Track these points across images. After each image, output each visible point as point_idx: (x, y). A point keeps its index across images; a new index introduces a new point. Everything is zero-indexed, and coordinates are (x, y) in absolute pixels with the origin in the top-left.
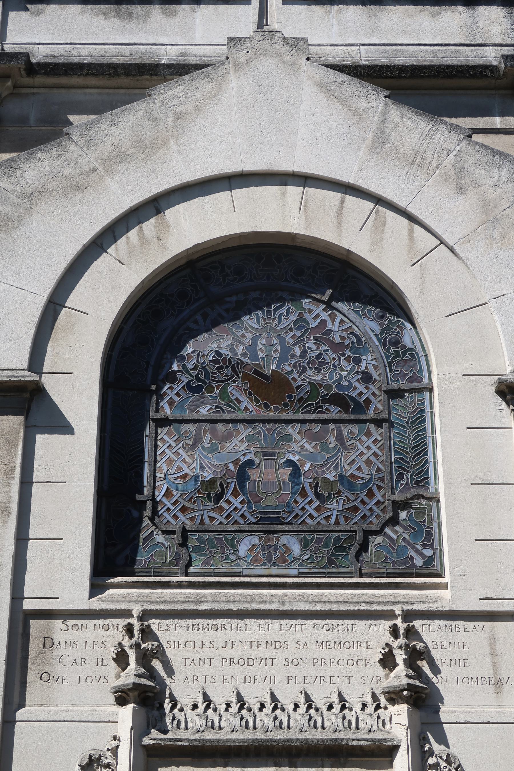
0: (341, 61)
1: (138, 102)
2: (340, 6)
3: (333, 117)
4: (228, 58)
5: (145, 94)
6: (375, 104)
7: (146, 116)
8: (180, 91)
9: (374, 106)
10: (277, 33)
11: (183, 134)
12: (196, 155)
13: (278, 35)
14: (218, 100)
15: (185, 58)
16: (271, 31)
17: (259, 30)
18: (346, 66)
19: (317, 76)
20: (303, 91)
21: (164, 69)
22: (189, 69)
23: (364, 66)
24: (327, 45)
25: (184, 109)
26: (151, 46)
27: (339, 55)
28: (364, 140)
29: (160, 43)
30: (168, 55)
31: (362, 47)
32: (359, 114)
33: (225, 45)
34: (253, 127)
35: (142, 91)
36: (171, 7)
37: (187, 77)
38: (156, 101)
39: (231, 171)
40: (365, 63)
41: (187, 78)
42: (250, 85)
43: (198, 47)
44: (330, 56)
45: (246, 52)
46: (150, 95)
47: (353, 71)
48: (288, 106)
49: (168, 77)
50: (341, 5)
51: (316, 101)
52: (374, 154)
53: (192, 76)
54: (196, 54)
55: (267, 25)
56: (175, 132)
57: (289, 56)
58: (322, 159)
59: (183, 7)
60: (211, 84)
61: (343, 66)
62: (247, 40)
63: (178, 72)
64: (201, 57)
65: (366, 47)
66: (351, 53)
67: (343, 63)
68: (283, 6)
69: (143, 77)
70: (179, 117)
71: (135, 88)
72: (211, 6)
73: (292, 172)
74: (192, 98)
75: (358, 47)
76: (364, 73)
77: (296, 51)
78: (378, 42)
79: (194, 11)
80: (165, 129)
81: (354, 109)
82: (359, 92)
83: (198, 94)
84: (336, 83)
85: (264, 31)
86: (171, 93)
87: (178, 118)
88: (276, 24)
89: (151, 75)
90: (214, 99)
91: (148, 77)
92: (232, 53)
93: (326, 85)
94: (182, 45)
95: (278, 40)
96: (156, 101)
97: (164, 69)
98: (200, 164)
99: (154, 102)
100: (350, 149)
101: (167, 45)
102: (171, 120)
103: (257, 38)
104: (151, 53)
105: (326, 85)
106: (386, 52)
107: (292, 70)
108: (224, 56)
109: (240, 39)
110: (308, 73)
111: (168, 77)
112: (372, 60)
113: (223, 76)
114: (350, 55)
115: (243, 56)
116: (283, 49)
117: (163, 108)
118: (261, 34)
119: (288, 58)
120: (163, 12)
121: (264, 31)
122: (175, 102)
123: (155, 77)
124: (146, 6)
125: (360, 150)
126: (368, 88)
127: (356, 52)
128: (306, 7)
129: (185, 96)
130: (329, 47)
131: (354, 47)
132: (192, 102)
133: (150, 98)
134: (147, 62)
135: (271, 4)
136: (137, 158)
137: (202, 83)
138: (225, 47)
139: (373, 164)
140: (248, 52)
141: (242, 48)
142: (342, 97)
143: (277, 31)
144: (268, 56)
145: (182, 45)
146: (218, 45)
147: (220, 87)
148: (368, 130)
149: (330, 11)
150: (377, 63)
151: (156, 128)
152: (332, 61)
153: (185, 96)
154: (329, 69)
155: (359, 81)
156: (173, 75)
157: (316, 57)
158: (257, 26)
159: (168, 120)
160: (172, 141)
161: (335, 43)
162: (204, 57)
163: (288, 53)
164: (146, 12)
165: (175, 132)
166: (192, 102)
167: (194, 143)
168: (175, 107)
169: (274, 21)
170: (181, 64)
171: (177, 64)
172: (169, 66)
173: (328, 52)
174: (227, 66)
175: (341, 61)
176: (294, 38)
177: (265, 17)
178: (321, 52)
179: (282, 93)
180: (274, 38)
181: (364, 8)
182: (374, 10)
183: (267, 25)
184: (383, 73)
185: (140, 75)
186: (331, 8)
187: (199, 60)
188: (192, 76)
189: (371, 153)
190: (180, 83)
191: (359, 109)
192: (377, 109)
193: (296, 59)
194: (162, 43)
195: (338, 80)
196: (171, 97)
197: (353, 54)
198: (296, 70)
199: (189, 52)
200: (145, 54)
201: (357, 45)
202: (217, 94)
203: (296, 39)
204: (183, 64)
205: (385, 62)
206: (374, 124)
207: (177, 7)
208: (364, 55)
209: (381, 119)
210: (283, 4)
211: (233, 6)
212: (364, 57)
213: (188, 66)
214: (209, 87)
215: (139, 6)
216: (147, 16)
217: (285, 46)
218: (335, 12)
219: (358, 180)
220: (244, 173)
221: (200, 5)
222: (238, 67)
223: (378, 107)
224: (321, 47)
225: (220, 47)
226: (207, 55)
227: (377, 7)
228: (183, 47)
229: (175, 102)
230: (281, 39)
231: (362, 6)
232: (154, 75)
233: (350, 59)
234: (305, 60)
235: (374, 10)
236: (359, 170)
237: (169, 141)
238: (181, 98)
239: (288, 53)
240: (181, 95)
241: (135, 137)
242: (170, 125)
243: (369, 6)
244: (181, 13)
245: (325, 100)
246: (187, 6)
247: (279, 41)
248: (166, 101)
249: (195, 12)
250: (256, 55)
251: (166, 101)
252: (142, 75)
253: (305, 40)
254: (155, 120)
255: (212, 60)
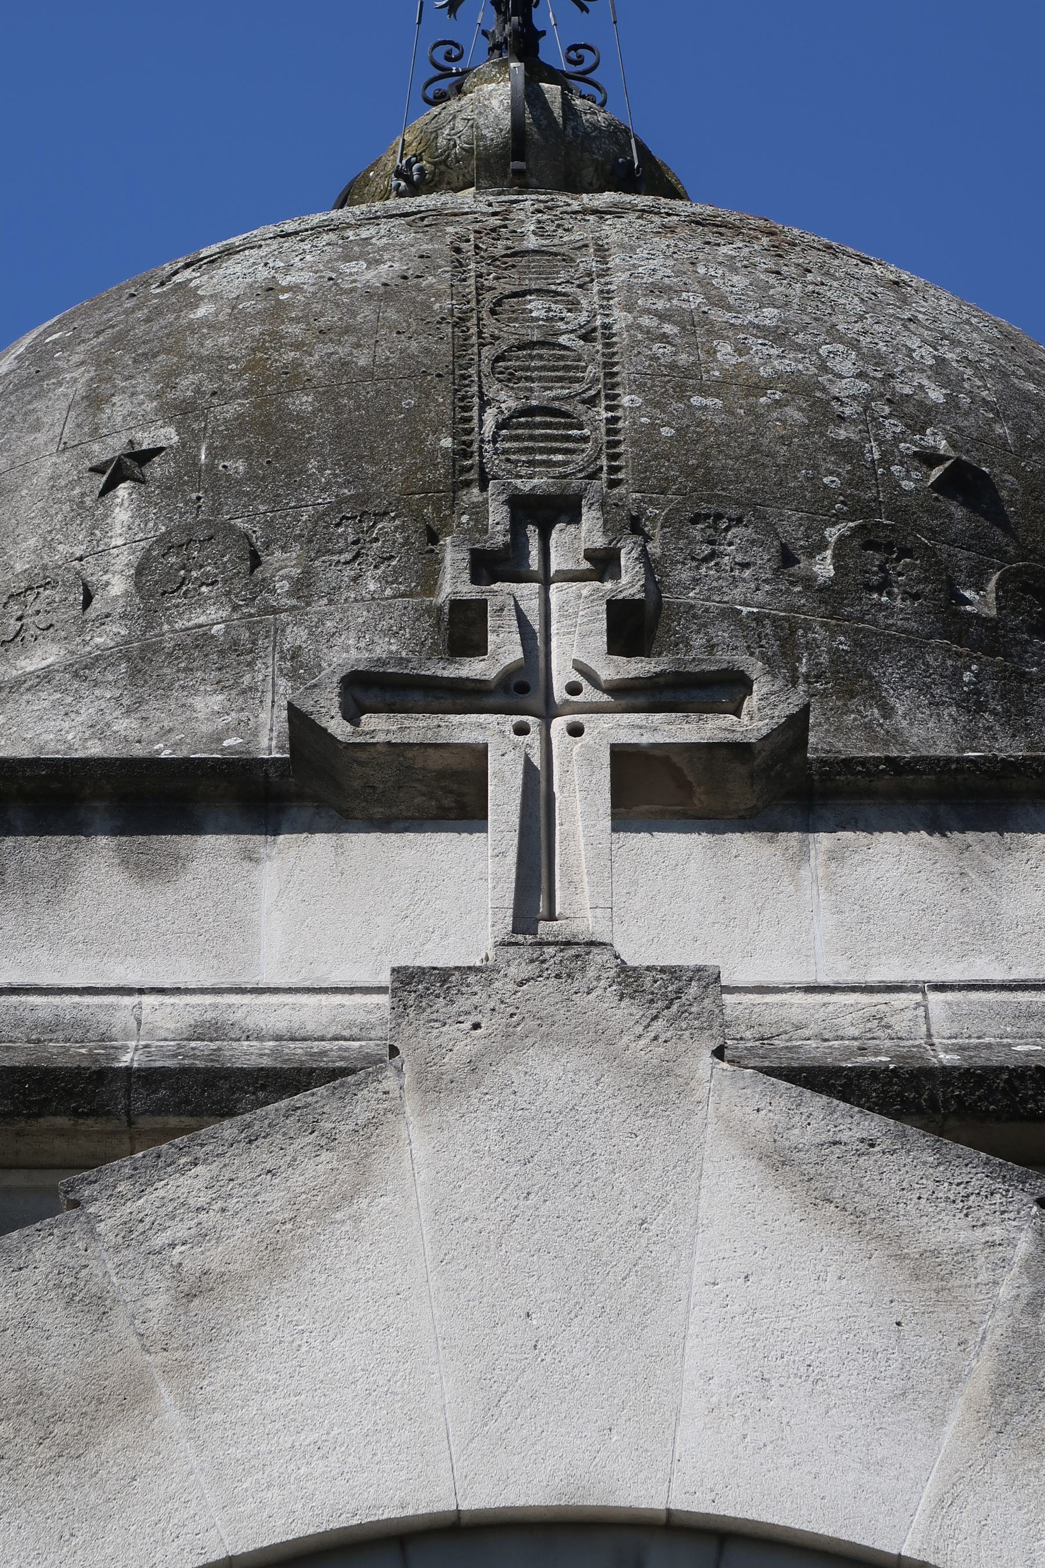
0: (852, 1054)
1: (26, 1231)
2: (840, 834)
3: (828, 1286)
4: (394, 1051)
5: (54, 1191)
6: (997, 1232)
7: (57, 1286)
8: (199, 1183)
9: (997, 1239)
10: (595, 950)
11: (210, 1361)
12: (263, 1448)
13: (598, 957)
14: (357, 1219)
15: (213, 1045)
16: (568, 944)
17: (520, 938)
18: (873, 1073)
19: (760, 1121)
20: (704, 1182)
21: (128, 1091)
22: (232, 1090)
23: (946, 1071)
24: (792, 989)
25: (214, 1257)
26: (76, 999)
27: (835, 1027)
28: (957, 1381)
29: (113, 984)
30: (147, 1032)
31: (934, 997)
32: (933, 1272)
33: (380, 990)
34: (499, 1330)
35: (40, 1179)
36: (157, 842)
37: (228, 1128)
38: (101, 1228)
39: (410, 1511)
40: (948, 1059)
41: (226, 1134)
42: (487, 1160)
43: (266, 998)
44: (807, 1032)
45: (467, 1026)
46: (76, 1204)
47: (900, 1094)
48: (644, 1242)
49: (145, 1123)
50: (844, 829)
51: (759, 1220)
52: (1003, 1438)
53: (249, 1126)
54: (266, 1026)
55: (551, 917)
56: (179, 1354)
57: (642, 1042)
58: (788, 1461)
59: (209, 841)
60: (325, 1156)
61: (860, 1072)
62: (472, 979)
63: (188, 1102)
64: (278, 1038)
65: (949, 996)
66: (892, 1021)
67: (861, 1061)
68: (616, 835)
69: (44, 1122)
70: (193, 1290)
71: (10, 1167)
72: (321, 839)
73: (664, 1516)
74: (247, 1214)
75: (918, 997)
76: (946, 1101)
77: (672, 1021)
78: (998, 975)
79: (250, 857)
80: (134, 1340)
81: (913, 1251)
82: (931, 1185)
83: (275, 1197)
84: (838, 1150)
85: (541, 944)
86: (161, 1193)
87: (190, 1296)
88: (589, 913)
89: (76, 1113)
90: (338, 1216)
91: (62, 1122)
92: (411, 1030)
93: (796, 1155)
94: (203, 991)
95: (598, 978)
96: (101, 1228)
97: (128, 1091)
98: (282, 1486)
99: (92, 1230)
100: (904, 1415)
101: (141, 991)
102: (159, 1302)
103: (513, 970)
104: (75, 1024)
105: (796, 1155)
106: (1031, 1016)
107: (656, 1098)
108: (373, 1034)
109: (444, 975)
110: (723, 1109)
111: (145, 1123)
112: (976, 1047)
113: (374, 1123)
114: (888, 1027)
115: (459, 1044)
116: (619, 1012)
117: (129, 1254)
118: (528, 953)
119: (640, 1051)
120: (125, 862)
121: (541, 944)
122: (179, 1230)
123: (90, 1121)
124: (58, 839)
125: (944, 1422)
126: (971, 1171)
127: (909, 1014)
128: (705, 838)
129: (220, 1204)
130: (799, 998)
131: (903, 996)
132: (249, 1229)
133: (74, 1213)
134: (61, 1062)
135: (569, 836)
136: (19, 1462)
137: (290, 1151)
138: (384, 999)
139: (1000, 1479)
140: (476, 1026)
141: (454, 1009)
142: (865, 1203)
143: (592, 944)
144: (559, 1041)
145: (203, 991)
146: (351, 990)
147: (362, 1165)
148: (974, 1339)
149: (803, 856)
150: (996, 1060)
151: (98, 1336)
152: (813, 1051)
153: (220, 1204)
154: (808, 1093)
155: (931, 1138)
156: (167, 1112)
157: (748, 1034)
158: (509, 920)
159: (150, 1303)
160: (163, 1389)
161: (824, 980)
162: (293, 1039)
163: (639, 1029)
164: (58, 863)
165: (179, 1354)
166: (249, 1229)
167: (258, 1398)
168: (180, 1248)
169: (580, 901)
170: (198, 1070)
171: (184, 1071)
172: (148, 1078)
173: (796, 1015)
174: (390, 1083)
175: (850, 1053)
176: (663, 970)
177: (544, 885)
178: (768, 1017)
179: (616, 1191)
180: (583, 969)
181: (936, 840)
182: (977, 848)
183: (551, 917)
184: (1024, 1101)
185: (29, 1116)
186: (804, 844)
187: (274, 1053)
188: (249, 1126)
189: (992, 1435)
190: (201, 1153)
191: (936, 1253)
192: (1008, 1253)
193: (671, 1056)
194: (122, 983)
195: (844, 1137)
196: (162, 1211)
197: (900, 1024)
198: (673, 1096)
199: (233, 1018)
200: (53, 1027)
201: (914, 989)
202: (348, 1198)
203: (673, 972)
204: (207, 1070)
205: (1028, 1054)
206: (999, 1315)
207: (184, 842)
208: (941, 1026)
209: (1027, 1291)
210: (615, 829)
211: (411, 836)
212: (944, 1032)
213: (226, 1078)
214: (314, 1169)
215: (29, 840)
216: (61, 877)
217: (626, 1001)
218: (822, 858)
219: (941, 1544)
220: (465, 1520)
221: (276, 833)
222: (435, 1086)
223: (1012, 1243)
224: (770, 998)
225: (358, 999)
226: (302, 1033)
227: (991, 837)
228: (208, 999)
229: (179, 1230)
230: (612, 973)
231: (930, 834)
232: (86, 1115)
233: (888, 1043)
234: (707, 1058)
235: (977, 848)
236: (943, 1503)
237: (150, 1389)
238: (203, 1216)
239: (639, 1029)
240: (202, 1201)
241: (11, 1375)
242: (155, 1324)
243: (956, 835)
244: (200, 867)
245: (795, 1217)
246: (224, 838)
247: (603, 983)
248: (141, 1227)
249: (257, 861)
250: (510, 1040)
251: (141, 1227)
252: (39, 1115)
253: (709, 979)
254: (97, 1306)
255: (323, 1053)
